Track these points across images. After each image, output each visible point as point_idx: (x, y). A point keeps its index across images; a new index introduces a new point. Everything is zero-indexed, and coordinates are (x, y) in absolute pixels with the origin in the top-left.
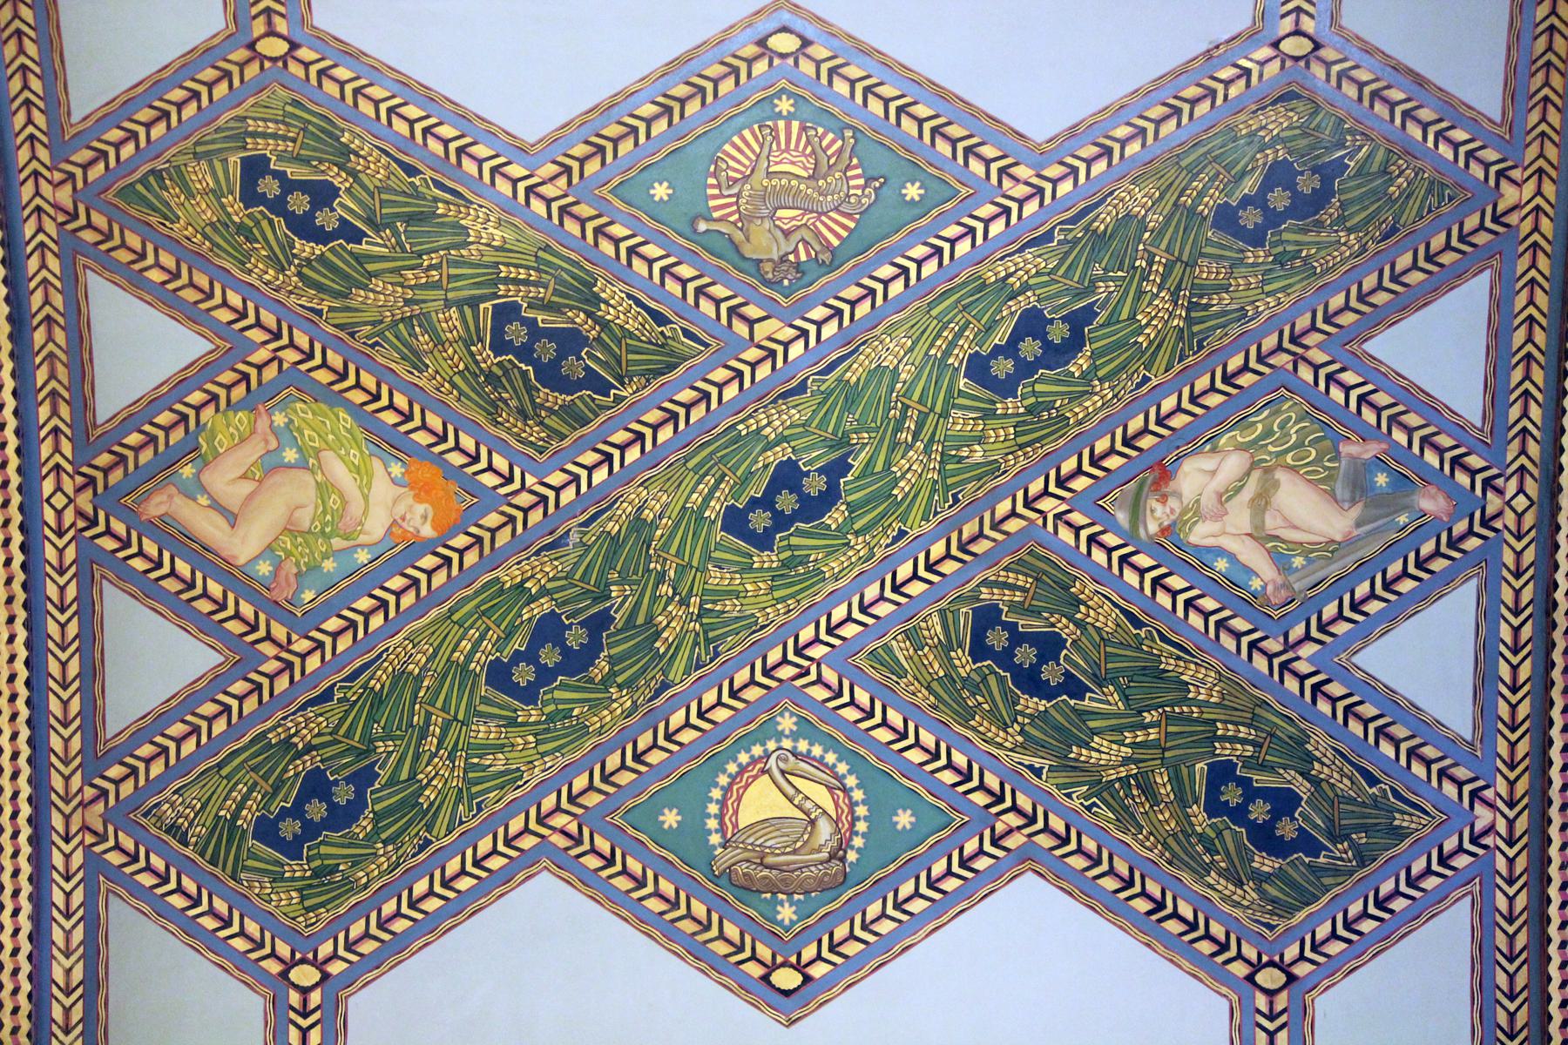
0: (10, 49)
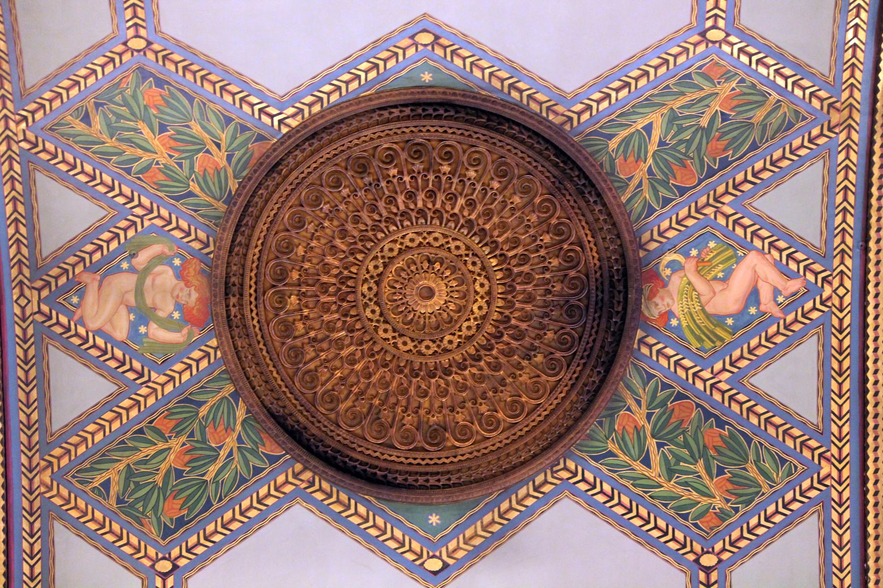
0: (7, 188)
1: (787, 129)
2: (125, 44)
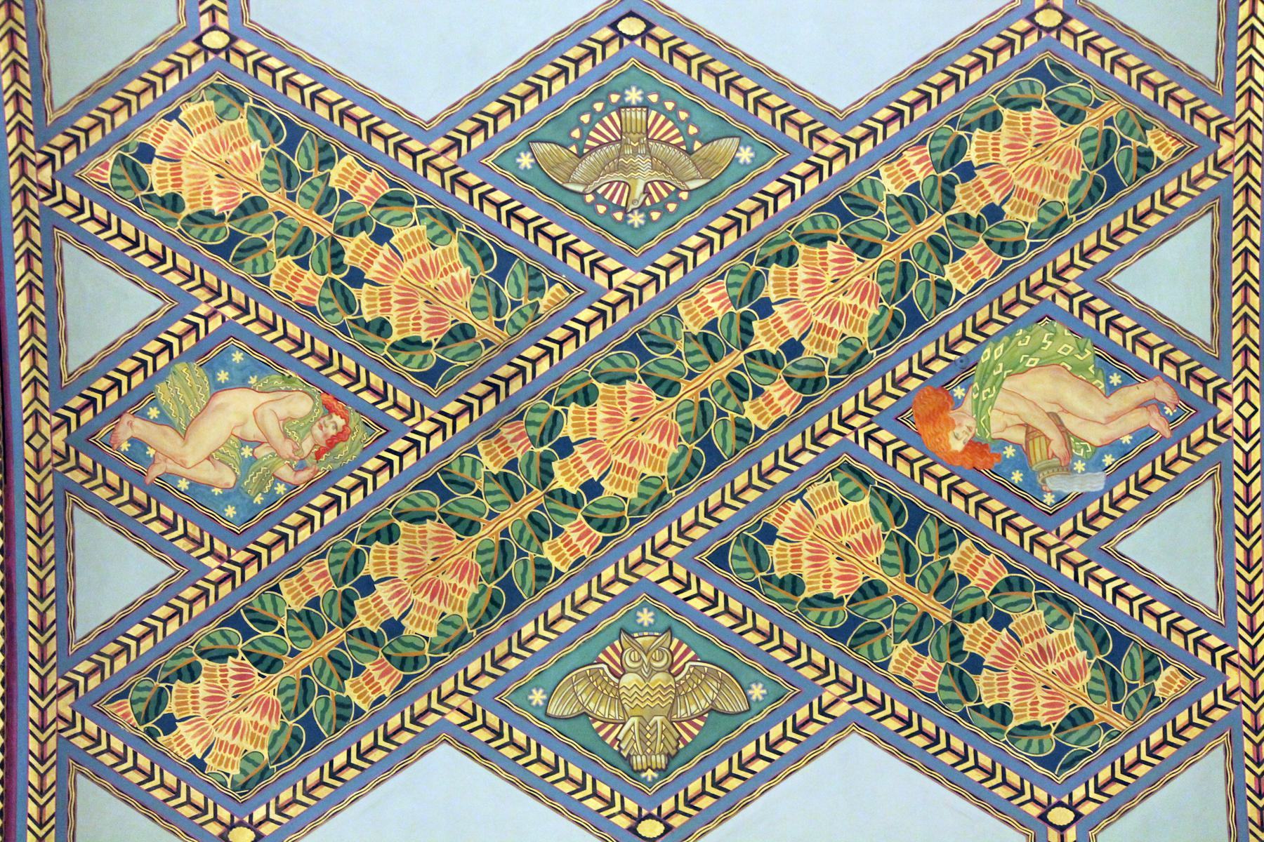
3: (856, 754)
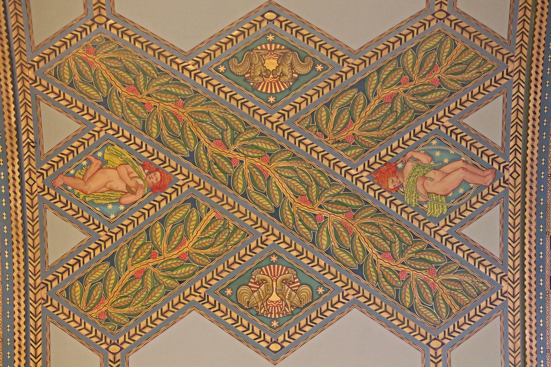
1: (177, 80)
2: (433, 15)
3: (355, 324)
